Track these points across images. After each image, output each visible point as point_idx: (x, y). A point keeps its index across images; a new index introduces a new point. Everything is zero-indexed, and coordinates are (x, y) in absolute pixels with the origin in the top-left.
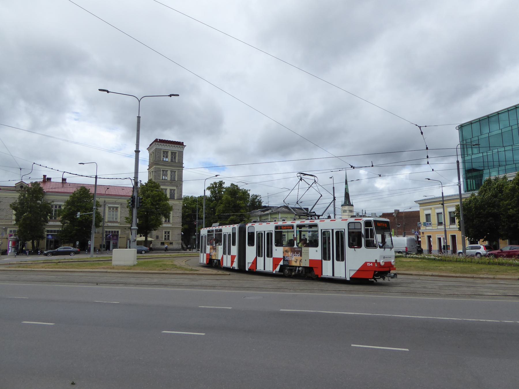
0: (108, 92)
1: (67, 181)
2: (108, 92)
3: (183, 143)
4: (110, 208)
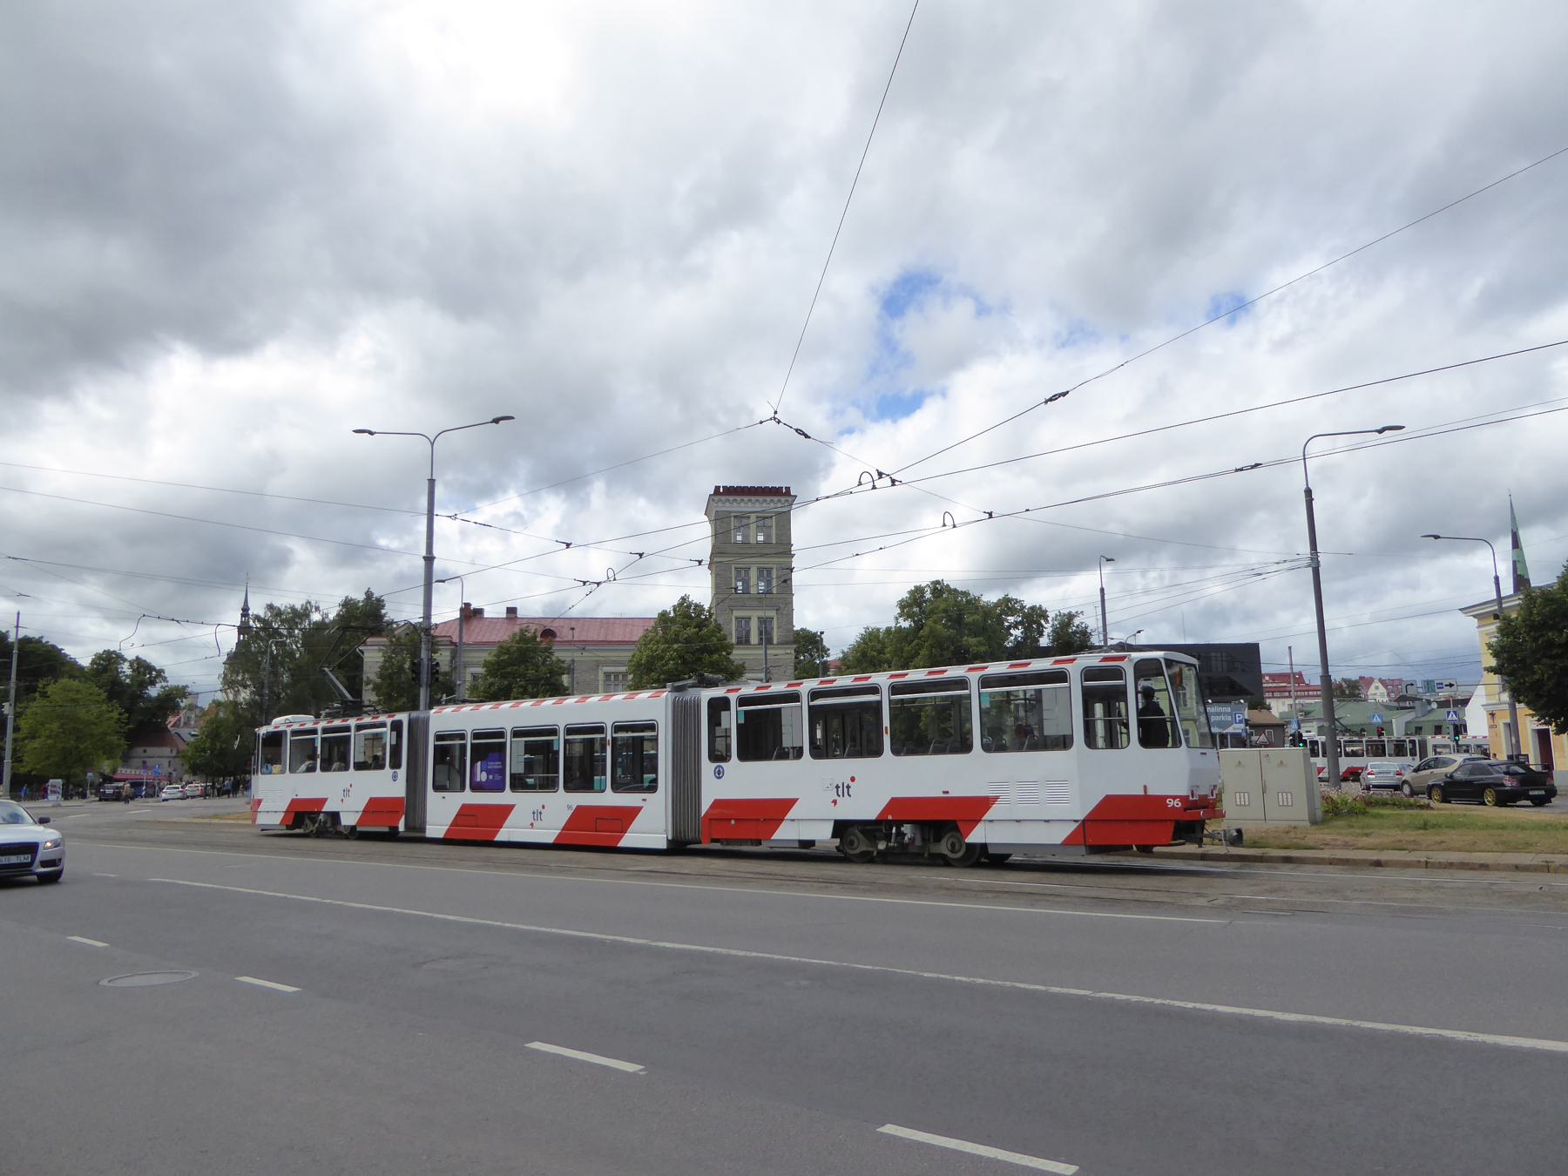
0: (371, 433)
1: (520, 614)
2: (371, 433)
3: (788, 489)
4: (607, 675)
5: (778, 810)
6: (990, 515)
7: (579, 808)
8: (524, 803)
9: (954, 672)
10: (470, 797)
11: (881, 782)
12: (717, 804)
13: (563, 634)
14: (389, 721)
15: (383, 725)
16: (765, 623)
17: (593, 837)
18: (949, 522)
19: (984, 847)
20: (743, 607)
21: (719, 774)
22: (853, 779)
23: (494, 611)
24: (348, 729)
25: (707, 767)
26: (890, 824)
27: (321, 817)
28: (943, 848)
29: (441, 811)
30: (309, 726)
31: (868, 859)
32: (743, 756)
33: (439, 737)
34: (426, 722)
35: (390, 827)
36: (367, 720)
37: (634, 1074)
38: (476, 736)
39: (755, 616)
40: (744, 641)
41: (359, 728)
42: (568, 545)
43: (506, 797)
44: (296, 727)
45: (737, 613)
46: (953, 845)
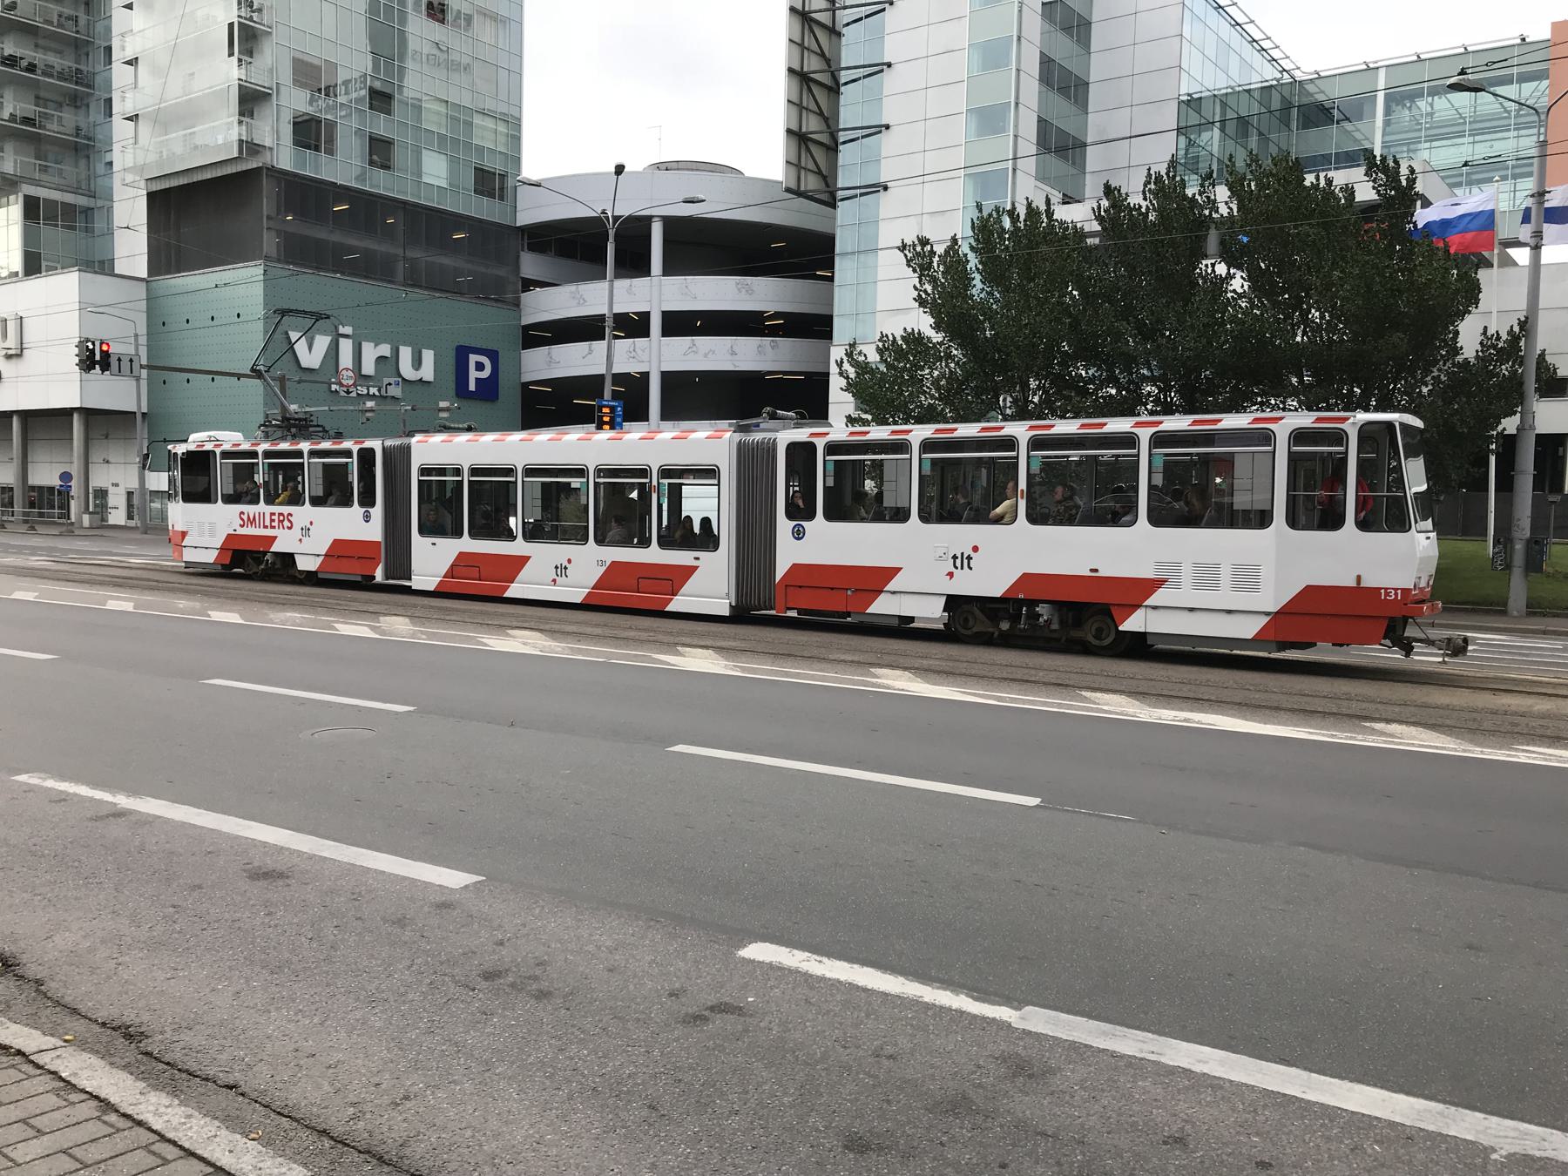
5: (877, 579)
7: (615, 565)
8: (544, 555)
9: (1118, 425)
10: (467, 544)
11: (1011, 553)
12: (796, 568)
14: (355, 449)
15: (348, 453)
17: (631, 602)
19: (1141, 637)
21: (799, 534)
22: (975, 549)
24: (299, 454)
25: (784, 525)
26: (1021, 602)
27: (268, 557)
28: (1088, 634)
29: (432, 559)
30: (246, 446)
32: (830, 516)
33: (424, 471)
34: (406, 451)
35: (351, 577)
36: (326, 445)
37: (445, 903)
38: (475, 471)
41: (313, 453)
43: (518, 547)
44: (227, 447)
46: (1100, 630)
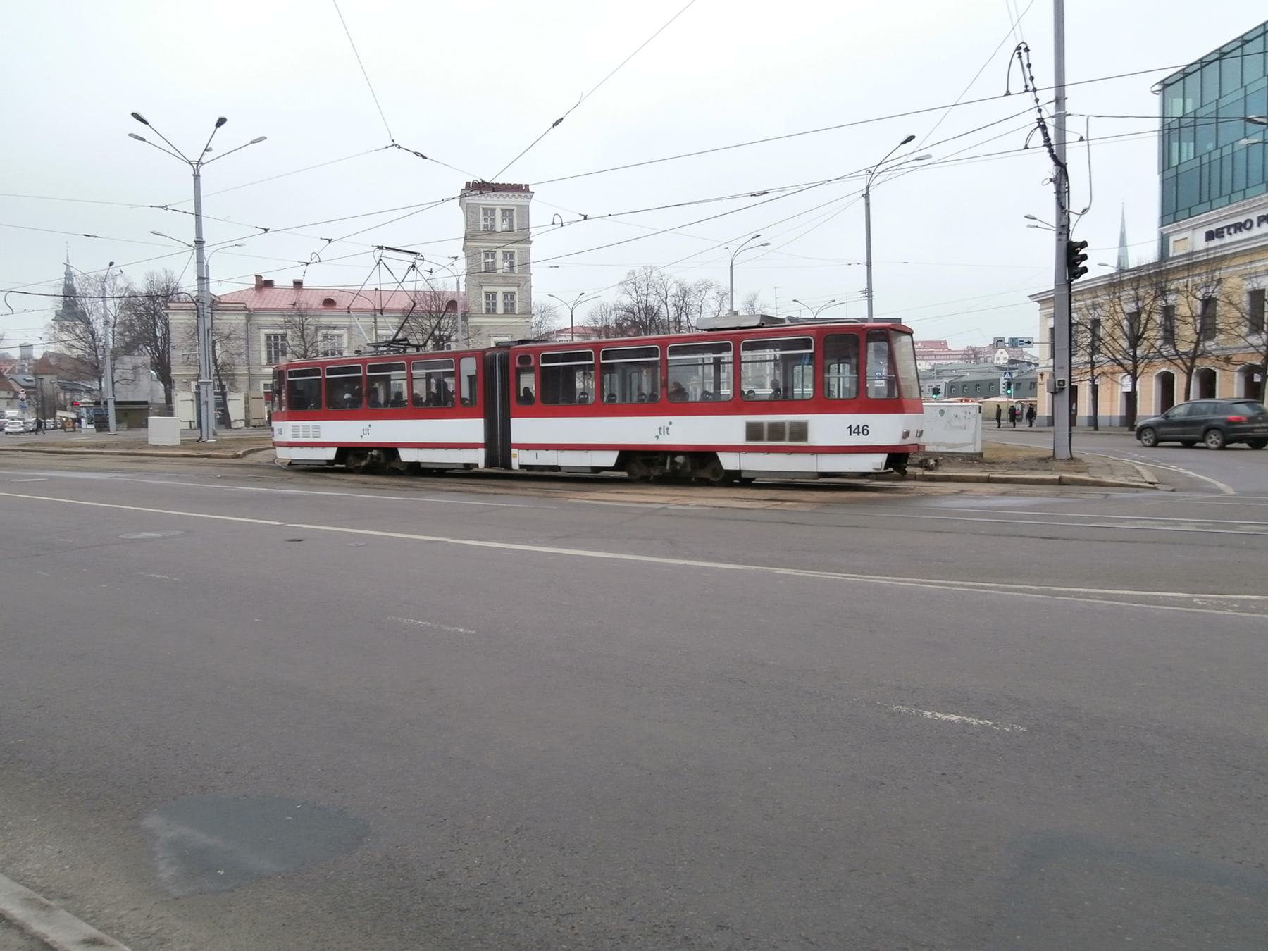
3: (527, 186)
6: (585, 217)
13: (343, 303)
16: (509, 297)
18: (557, 220)
20: (489, 284)
23: (284, 281)
28: (705, 474)
31: (646, 481)
39: (500, 291)
40: (491, 310)
42: (266, 230)
45: (486, 289)
